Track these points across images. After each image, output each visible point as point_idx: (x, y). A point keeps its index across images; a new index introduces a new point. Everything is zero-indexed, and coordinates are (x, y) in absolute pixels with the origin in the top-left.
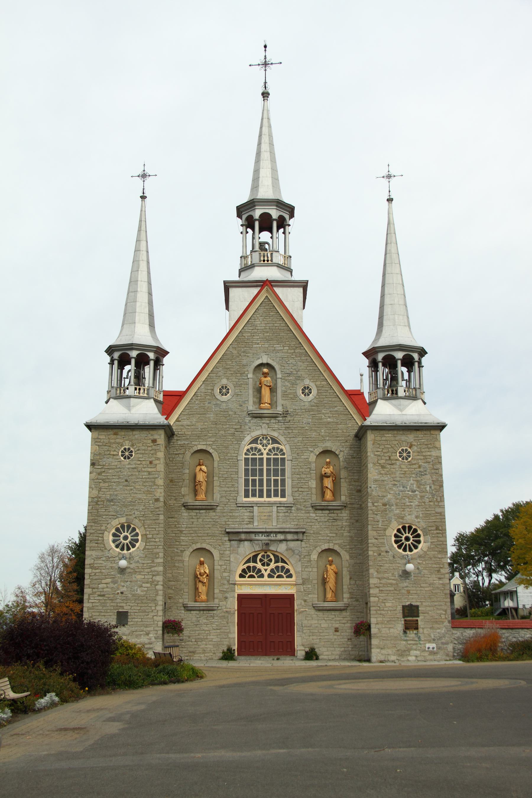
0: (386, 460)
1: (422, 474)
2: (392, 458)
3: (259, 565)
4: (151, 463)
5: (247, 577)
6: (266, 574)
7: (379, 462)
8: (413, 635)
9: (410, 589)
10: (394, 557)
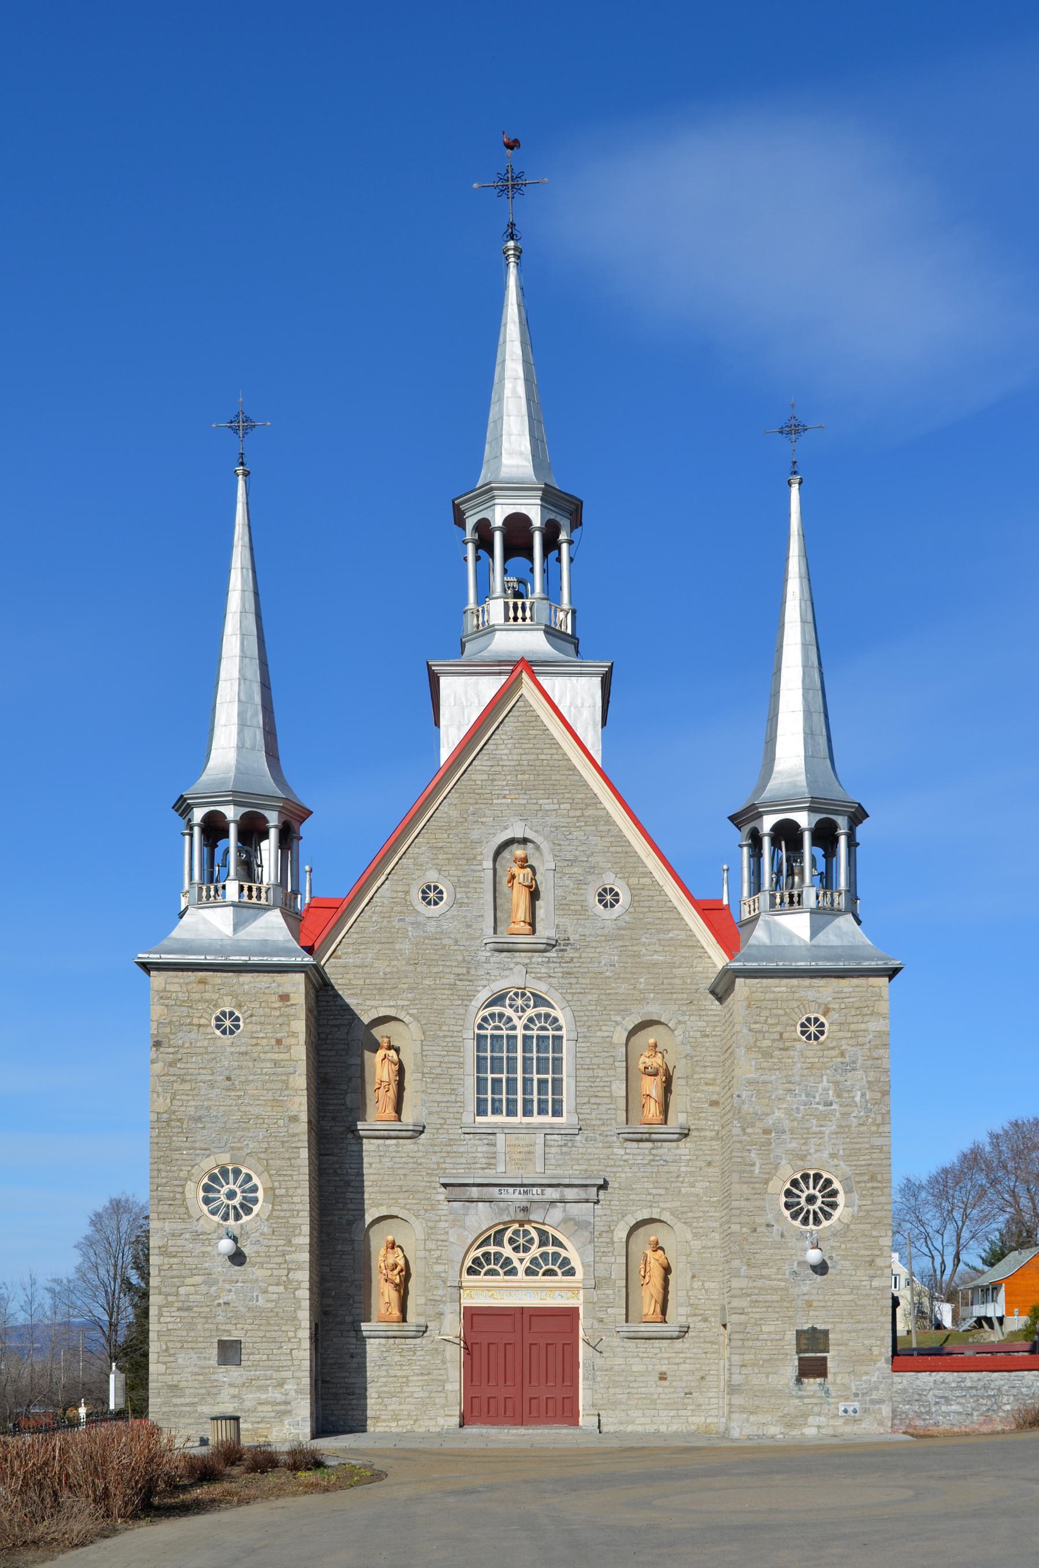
0: (774, 1040)
1: (849, 1067)
2: (785, 1035)
3: (507, 1251)
4: (279, 1042)
5: (482, 1274)
6: (521, 1268)
7: (758, 1044)
8: (816, 1387)
9: (813, 1297)
10: (782, 1236)
